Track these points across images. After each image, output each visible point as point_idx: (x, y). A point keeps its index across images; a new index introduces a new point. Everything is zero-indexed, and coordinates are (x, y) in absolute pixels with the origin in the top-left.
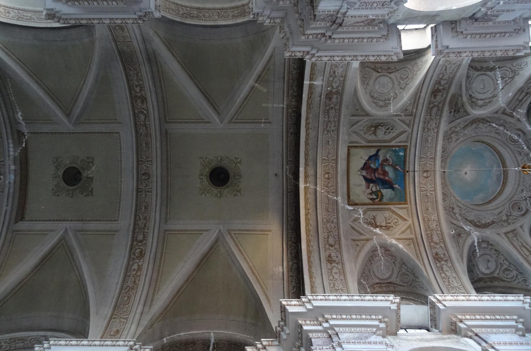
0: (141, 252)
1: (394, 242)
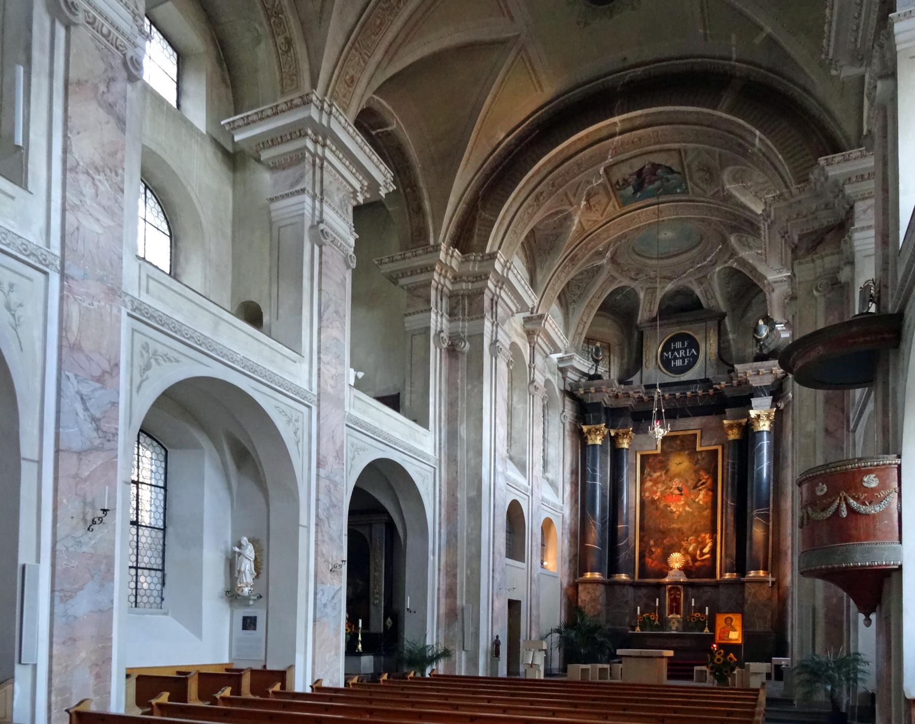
1: (576, 222)
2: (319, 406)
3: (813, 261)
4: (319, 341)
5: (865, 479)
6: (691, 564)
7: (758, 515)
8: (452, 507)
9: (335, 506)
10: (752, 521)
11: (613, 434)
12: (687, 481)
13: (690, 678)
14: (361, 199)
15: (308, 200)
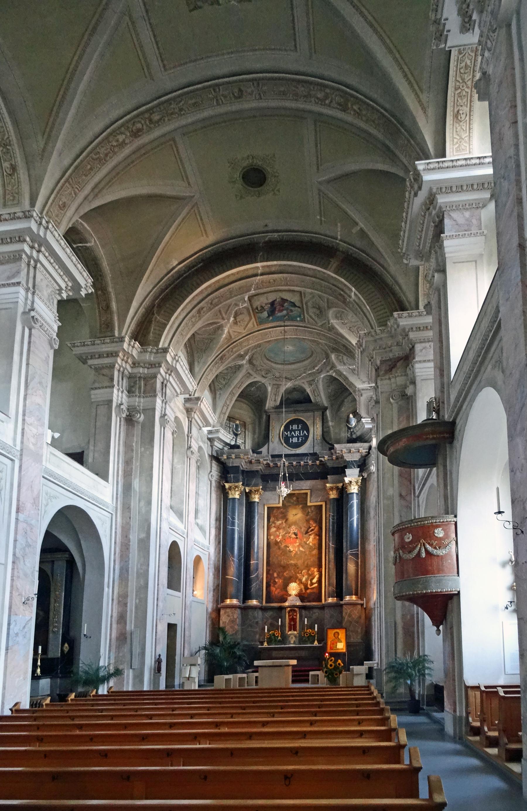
0: (139, 130)
1: (226, 331)
2: (21, 460)
3: (390, 379)
4: (25, 405)
5: (436, 531)
6: (304, 591)
7: (351, 554)
8: (125, 546)
9: (30, 545)
10: (347, 559)
11: (247, 491)
12: (301, 528)
13: (307, 681)
14: (64, 295)
15: (22, 292)
